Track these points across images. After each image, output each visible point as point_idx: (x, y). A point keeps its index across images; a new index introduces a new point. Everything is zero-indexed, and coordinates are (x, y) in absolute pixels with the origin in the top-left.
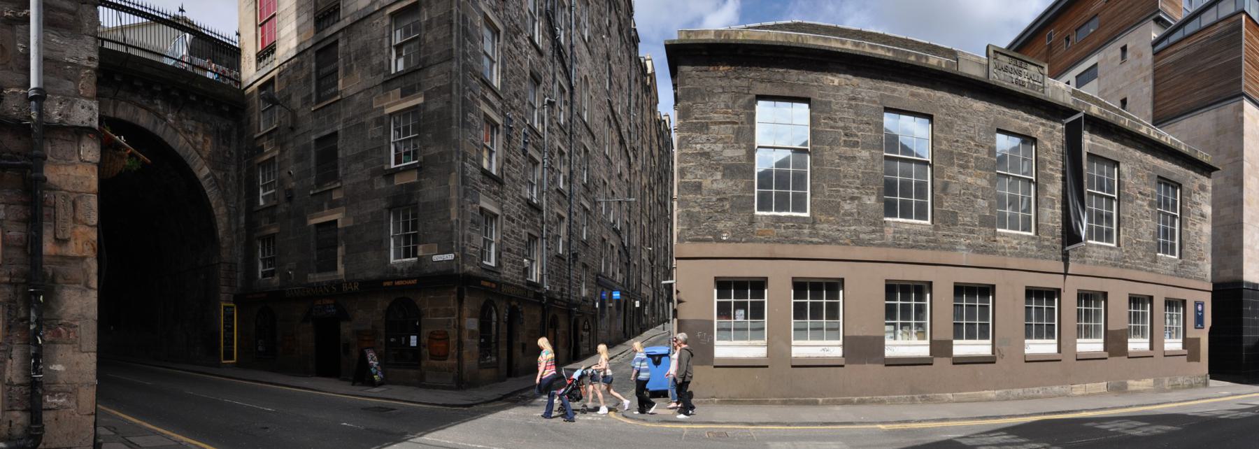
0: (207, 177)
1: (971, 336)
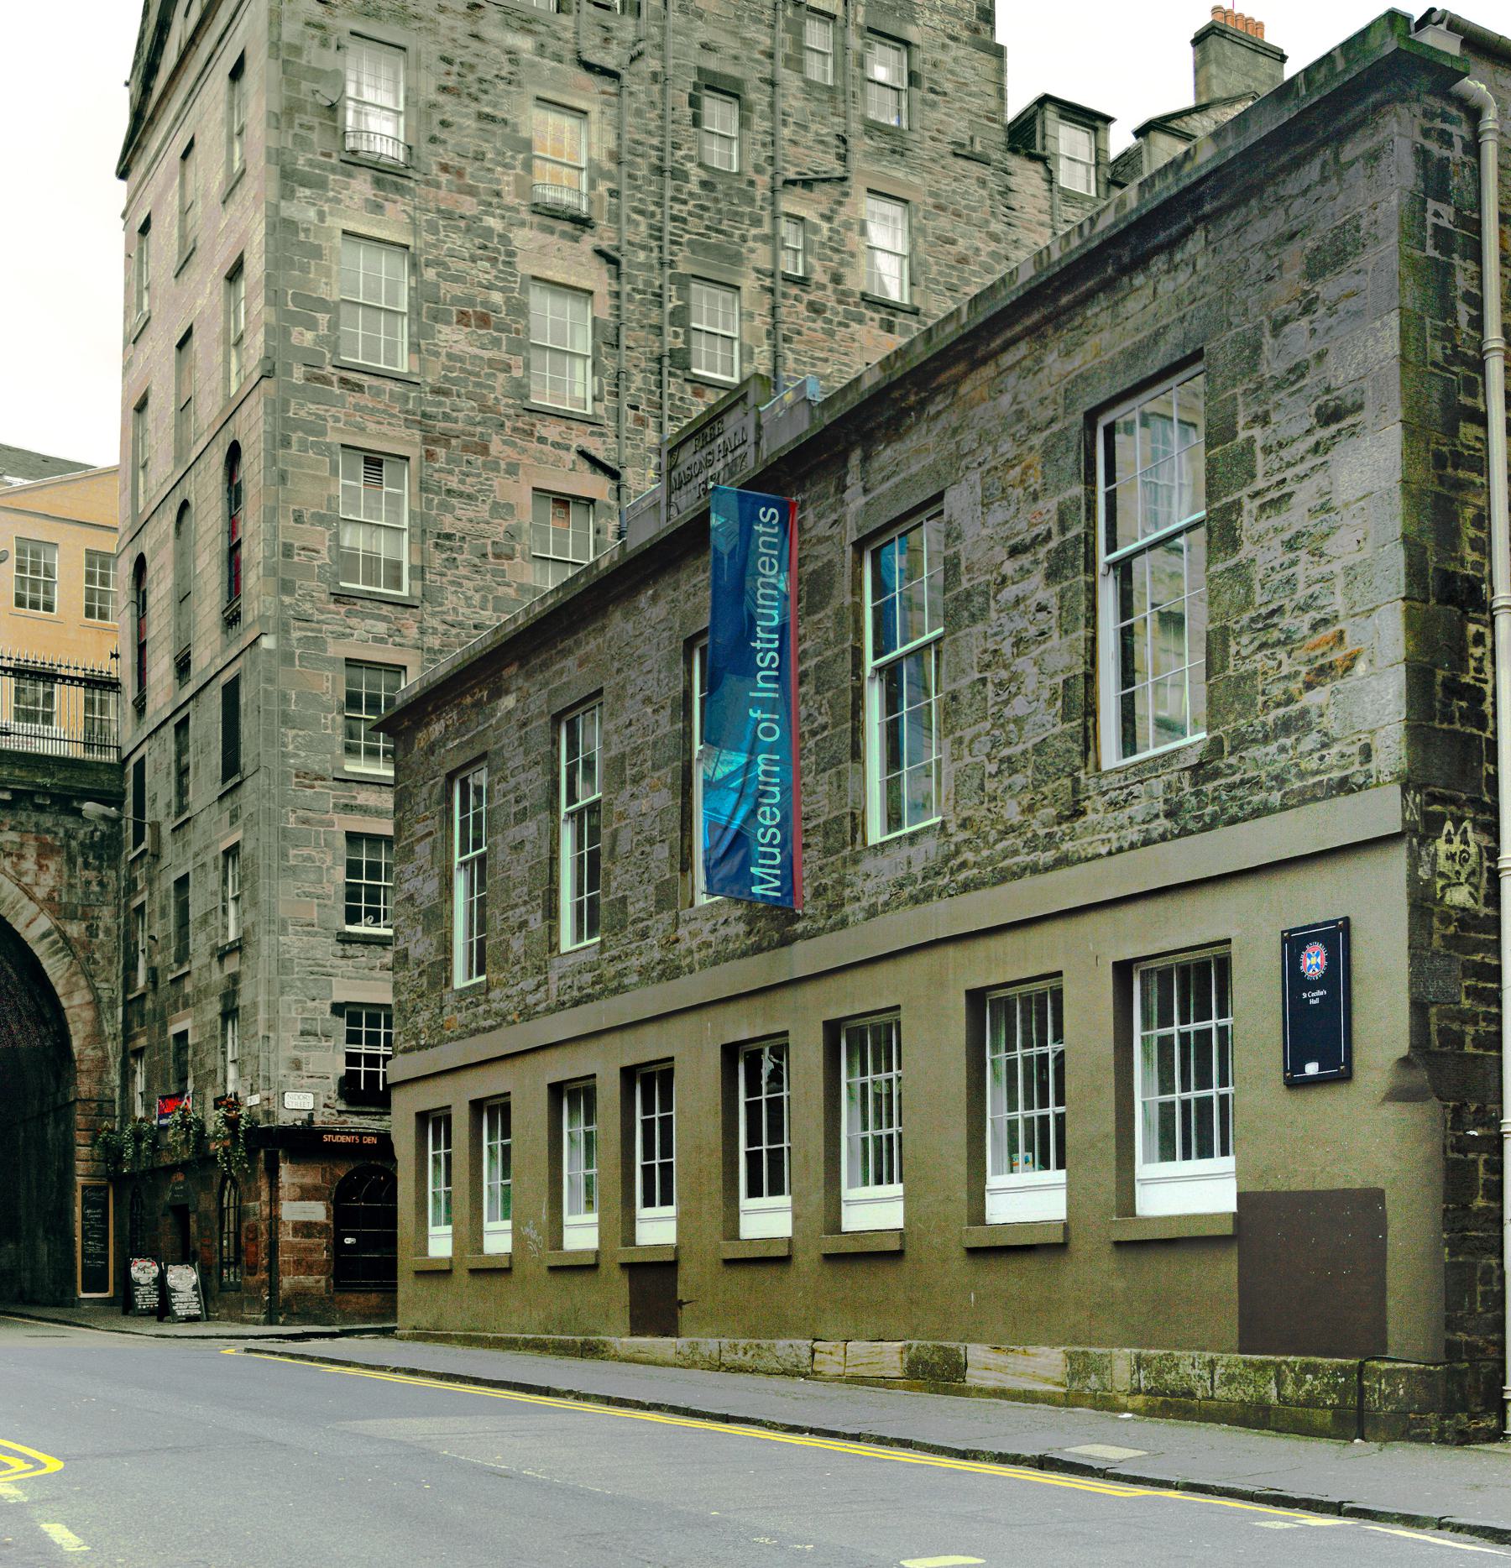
0: (45, 936)
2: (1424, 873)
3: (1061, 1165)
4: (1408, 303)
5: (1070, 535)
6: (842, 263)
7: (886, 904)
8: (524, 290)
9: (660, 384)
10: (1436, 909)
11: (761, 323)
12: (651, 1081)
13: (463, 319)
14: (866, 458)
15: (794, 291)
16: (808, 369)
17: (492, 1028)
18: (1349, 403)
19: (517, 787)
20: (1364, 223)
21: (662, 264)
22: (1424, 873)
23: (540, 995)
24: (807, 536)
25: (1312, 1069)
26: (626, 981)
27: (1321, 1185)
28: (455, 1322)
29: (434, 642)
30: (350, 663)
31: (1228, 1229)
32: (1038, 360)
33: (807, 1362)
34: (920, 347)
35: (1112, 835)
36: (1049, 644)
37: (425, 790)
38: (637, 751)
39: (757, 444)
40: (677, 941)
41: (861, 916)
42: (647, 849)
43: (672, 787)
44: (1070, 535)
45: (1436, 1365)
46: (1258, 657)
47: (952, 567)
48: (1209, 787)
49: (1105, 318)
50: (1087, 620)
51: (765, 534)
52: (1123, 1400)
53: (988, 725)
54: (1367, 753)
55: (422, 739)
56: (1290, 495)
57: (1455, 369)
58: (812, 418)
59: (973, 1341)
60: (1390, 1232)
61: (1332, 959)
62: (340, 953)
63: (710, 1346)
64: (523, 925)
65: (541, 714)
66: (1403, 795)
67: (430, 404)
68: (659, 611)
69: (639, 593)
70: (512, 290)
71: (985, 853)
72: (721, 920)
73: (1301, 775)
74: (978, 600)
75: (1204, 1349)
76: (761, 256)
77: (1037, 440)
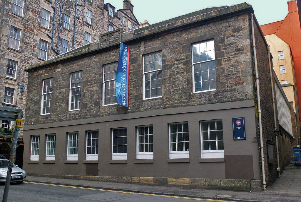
1: (213, 148)
6: (83, 17)
9: (59, 28)
11: (73, 22)
13: (32, 11)
16: (78, 30)
17: (52, 122)
18: (241, 49)
20: (243, 27)
21: (60, 11)
25: (239, 138)
27: (241, 154)
29: (23, 59)
30: (9, 59)
42: (93, 96)
46: (226, 80)
48: (217, 97)
54: (246, 95)
56: (231, 59)
68: (97, 60)
73: (234, 97)
76: (73, 13)
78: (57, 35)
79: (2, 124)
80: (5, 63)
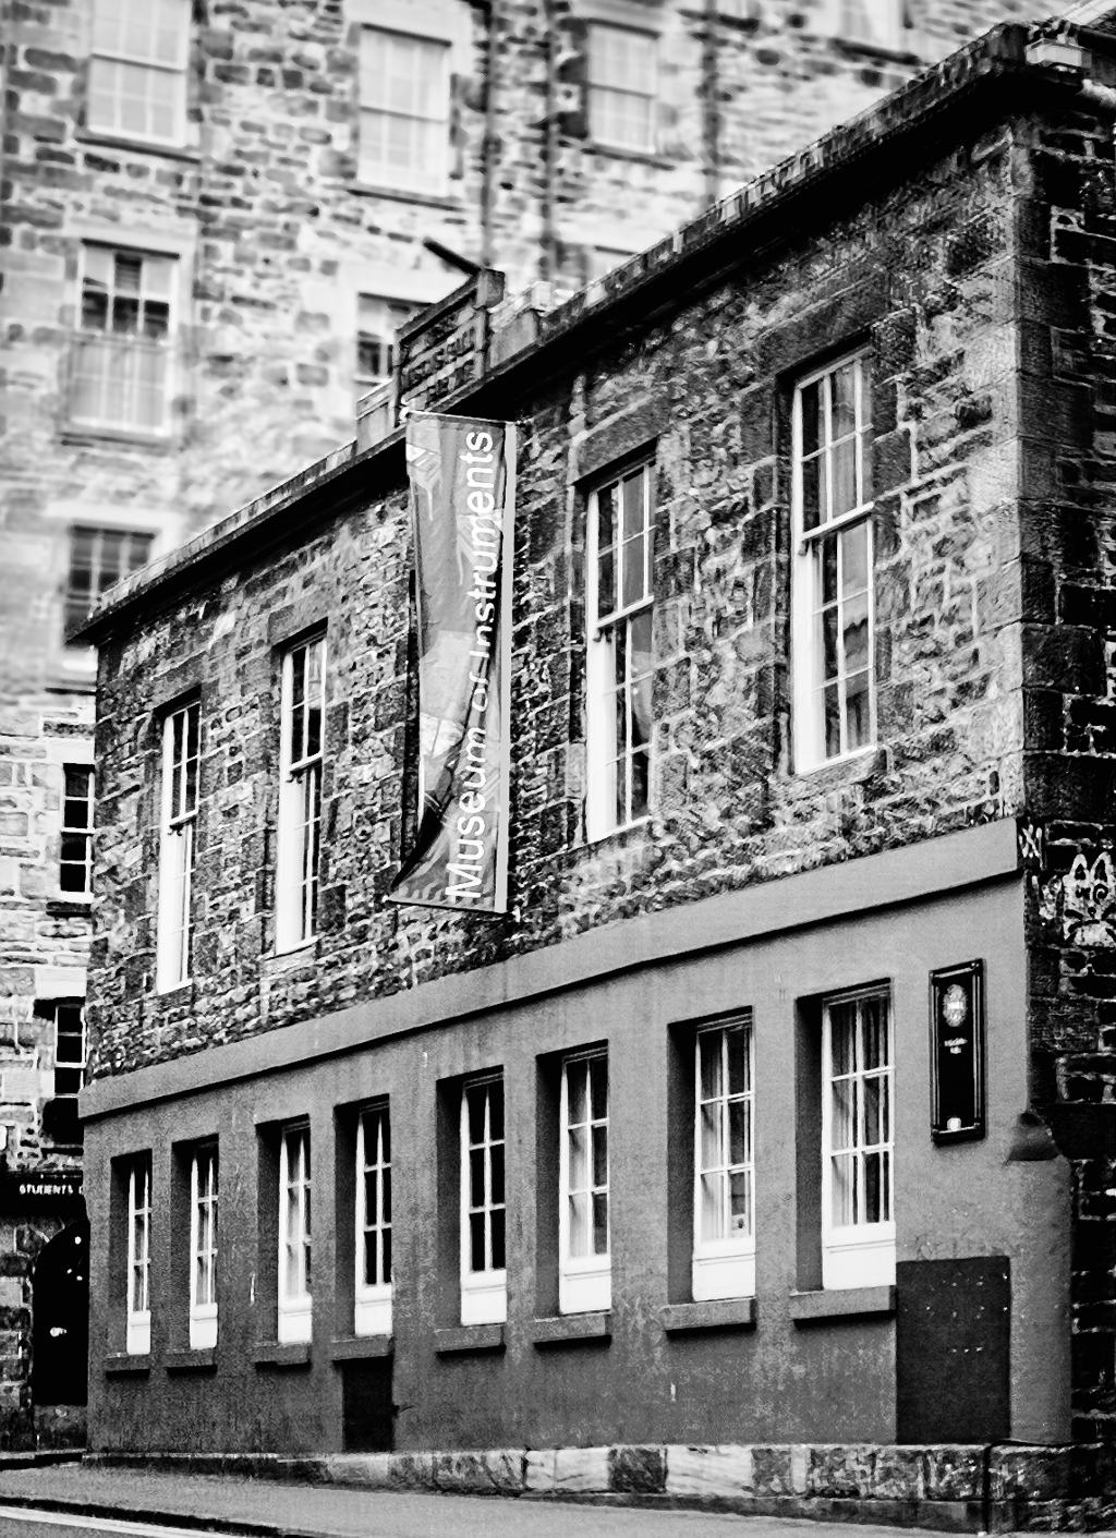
2: (1047, 912)
3: (499, 1262)
4: (1030, 315)
5: (764, 508)
7: (597, 916)
8: (353, 40)
10: (1063, 951)
12: (364, 1118)
13: (264, 78)
14: (589, 388)
15: (736, 36)
17: (197, 1049)
19: (231, 737)
22: (1047, 912)
23: (251, 1009)
24: (531, 468)
26: (343, 995)
28: (152, 1438)
31: (884, 1303)
32: (740, 309)
33: (518, 1476)
34: (638, 271)
35: (797, 852)
36: (743, 629)
37: (130, 727)
38: (360, 702)
39: (485, 350)
40: (396, 946)
41: (575, 927)
43: (393, 753)
44: (764, 508)
45: (1059, 1447)
47: (662, 523)
48: (876, 805)
49: (794, 278)
50: (779, 605)
51: (474, 465)
52: (802, 1504)
53: (691, 712)
55: (129, 659)
56: (937, 497)
57: (1091, 377)
58: (539, 330)
59: (673, 1441)
60: (1014, 1303)
61: (940, 1006)
62: (52, 931)
63: (425, 1459)
64: (234, 915)
65: (260, 643)
66: (1020, 832)
67: (213, 185)
69: (367, 507)
70: (335, 41)
71: (689, 862)
72: (440, 924)
73: (951, 800)
74: (684, 568)
75: (868, 1441)
77: (737, 398)
78: (531, 223)
79: (52, 1075)
80: (49, 560)
